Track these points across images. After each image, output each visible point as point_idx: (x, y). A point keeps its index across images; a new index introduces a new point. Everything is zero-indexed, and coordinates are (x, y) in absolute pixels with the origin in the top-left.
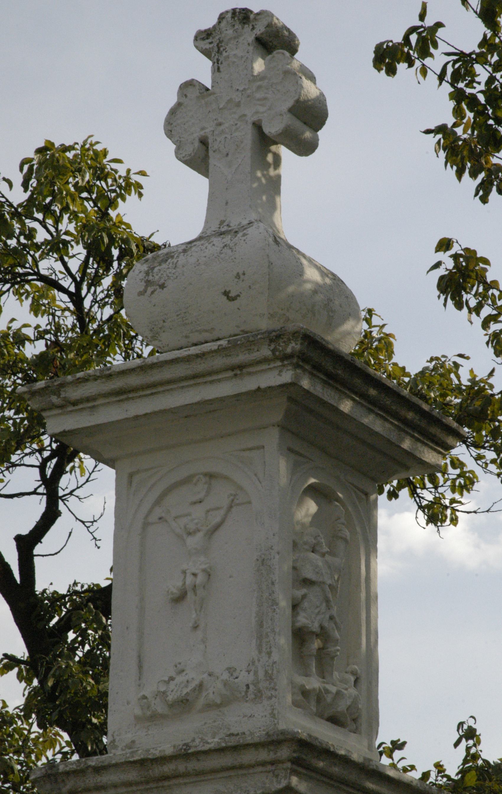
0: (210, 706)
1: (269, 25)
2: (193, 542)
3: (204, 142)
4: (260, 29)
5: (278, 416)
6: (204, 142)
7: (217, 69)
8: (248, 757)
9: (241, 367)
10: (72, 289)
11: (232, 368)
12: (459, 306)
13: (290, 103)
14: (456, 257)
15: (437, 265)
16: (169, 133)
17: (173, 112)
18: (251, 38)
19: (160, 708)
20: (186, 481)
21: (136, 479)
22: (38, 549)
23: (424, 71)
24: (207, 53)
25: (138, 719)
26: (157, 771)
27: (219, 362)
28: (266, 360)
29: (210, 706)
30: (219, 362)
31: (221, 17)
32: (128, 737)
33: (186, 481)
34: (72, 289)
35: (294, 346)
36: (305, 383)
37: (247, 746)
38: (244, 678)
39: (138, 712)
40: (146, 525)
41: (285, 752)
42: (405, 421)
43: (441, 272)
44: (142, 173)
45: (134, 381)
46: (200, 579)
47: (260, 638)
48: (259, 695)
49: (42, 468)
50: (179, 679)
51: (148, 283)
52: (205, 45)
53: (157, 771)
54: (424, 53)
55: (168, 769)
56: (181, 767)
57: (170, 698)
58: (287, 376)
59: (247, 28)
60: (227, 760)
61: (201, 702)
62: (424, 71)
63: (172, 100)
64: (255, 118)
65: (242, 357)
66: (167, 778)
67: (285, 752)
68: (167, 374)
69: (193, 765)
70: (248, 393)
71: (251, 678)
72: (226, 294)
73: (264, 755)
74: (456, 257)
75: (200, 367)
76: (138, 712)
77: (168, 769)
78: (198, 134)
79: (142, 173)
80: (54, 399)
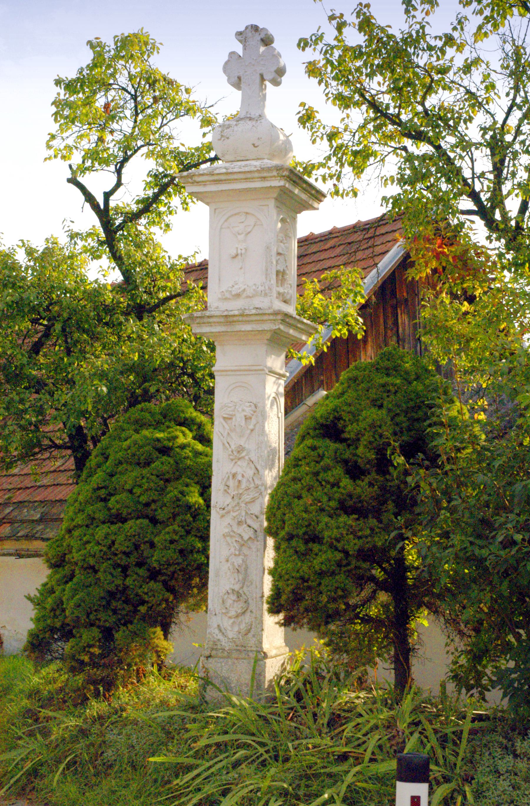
0: (248, 297)
1: (266, 34)
2: (241, 237)
3: (239, 78)
4: (262, 36)
5: (275, 195)
6: (239, 78)
7: (245, 49)
8: (266, 318)
9: (264, 178)
10: (133, 92)
11: (262, 177)
12: (304, 127)
13: (275, 68)
14: (307, 110)
15: (299, 113)
16: (225, 72)
17: (226, 63)
18: (259, 39)
19: (227, 295)
20: (238, 214)
21: (217, 211)
22: (111, 198)
23: (315, 49)
24: (241, 41)
25: (219, 299)
26: (231, 319)
27: (256, 175)
28: (274, 176)
29: (248, 297)
30: (256, 175)
31: (247, 28)
32: (216, 305)
33: (238, 214)
34: (133, 92)
35: (286, 173)
36: (287, 185)
37: (264, 314)
38: (261, 288)
39: (220, 296)
40: (221, 228)
41: (279, 317)
42: (312, 194)
43: (301, 115)
44: (161, 44)
45: (223, 177)
46: (243, 251)
47: (266, 274)
48: (266, 295)
49: (116, 166)
50: (236, 286)
51: (222, 136)
52: (240, 37)
53: (231, 319)
54: (316, 44)
55: (235, 319)
56: (241, 318)
57: (233, 293)
58: (282, 183)
59: (257, 34)
60: (258, 318)
61: (245, 295)
62: (315, 49)
63: (226, 58)
64: (261, 72)
65: (265, 175)
66: (233, 322)
67: (279, 317)
68: (235, 176)
69: (245, 319)
70: (266, 187)
71: (263, 288)
72: (254, 145)
73: (271, 317)
74: (307, 110)
75: (249, 176)
76: (220, 296)
77: (235, 319)
78: (237, 74)
79: (161, 44)
80: (190, 180)
